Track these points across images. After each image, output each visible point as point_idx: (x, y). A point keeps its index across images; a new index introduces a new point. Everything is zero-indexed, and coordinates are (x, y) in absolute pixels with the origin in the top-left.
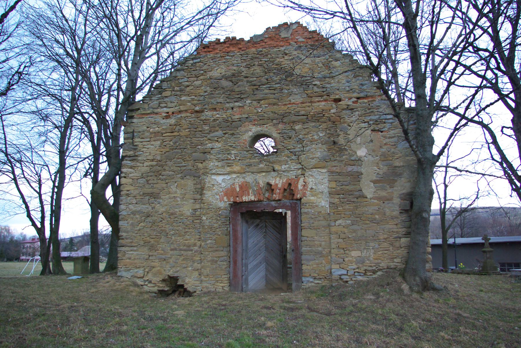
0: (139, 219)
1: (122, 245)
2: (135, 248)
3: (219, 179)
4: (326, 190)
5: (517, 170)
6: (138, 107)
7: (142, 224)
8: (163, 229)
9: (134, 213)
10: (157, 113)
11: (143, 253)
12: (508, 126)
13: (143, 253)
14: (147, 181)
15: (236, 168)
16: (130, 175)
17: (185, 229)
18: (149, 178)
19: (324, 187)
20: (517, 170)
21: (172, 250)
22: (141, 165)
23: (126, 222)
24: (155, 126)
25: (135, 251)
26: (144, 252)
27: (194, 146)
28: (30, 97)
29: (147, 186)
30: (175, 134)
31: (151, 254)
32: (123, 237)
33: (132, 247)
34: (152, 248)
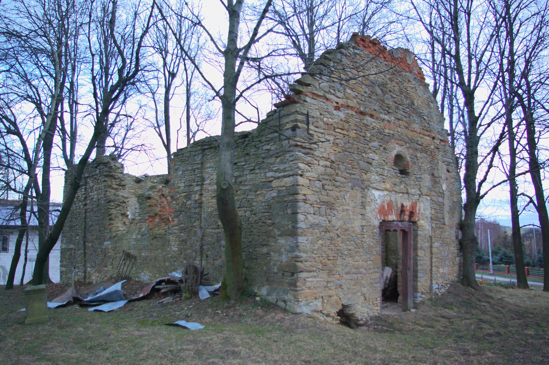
0: (318, 235)
1: (302, 270)
2: (315, 274)
3: (376, 193)
4: (429, 216)
5: (258, 123)
6: (309, 82)
7: (320, 242)
8: (339, 248)
9: (313, 226)
10: (327, 99)
11: (322, 280)
12: (489, 188)
13: (322, 280)
14: (323, 186)
15: (388, 186)
16: (308, 174)
17: (355, 248)
18: (324, 182)
19: (428, 213)
20: (258, 123)
21: (347, 273)
22: (317, 162)
23: (305, 238)
24: (329, 116)
25: (315, 277)
26: (324, 276)
27: (360, 152)
28: (131, 50)
29: (323, 192)
30: (345, 132)
31: (330, 280)
32: (302, 259)
33: (311, 272)
34: (330, 273)
